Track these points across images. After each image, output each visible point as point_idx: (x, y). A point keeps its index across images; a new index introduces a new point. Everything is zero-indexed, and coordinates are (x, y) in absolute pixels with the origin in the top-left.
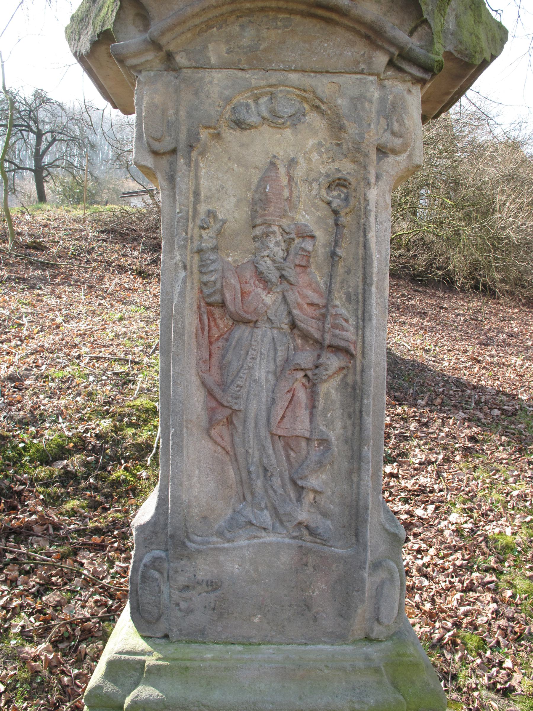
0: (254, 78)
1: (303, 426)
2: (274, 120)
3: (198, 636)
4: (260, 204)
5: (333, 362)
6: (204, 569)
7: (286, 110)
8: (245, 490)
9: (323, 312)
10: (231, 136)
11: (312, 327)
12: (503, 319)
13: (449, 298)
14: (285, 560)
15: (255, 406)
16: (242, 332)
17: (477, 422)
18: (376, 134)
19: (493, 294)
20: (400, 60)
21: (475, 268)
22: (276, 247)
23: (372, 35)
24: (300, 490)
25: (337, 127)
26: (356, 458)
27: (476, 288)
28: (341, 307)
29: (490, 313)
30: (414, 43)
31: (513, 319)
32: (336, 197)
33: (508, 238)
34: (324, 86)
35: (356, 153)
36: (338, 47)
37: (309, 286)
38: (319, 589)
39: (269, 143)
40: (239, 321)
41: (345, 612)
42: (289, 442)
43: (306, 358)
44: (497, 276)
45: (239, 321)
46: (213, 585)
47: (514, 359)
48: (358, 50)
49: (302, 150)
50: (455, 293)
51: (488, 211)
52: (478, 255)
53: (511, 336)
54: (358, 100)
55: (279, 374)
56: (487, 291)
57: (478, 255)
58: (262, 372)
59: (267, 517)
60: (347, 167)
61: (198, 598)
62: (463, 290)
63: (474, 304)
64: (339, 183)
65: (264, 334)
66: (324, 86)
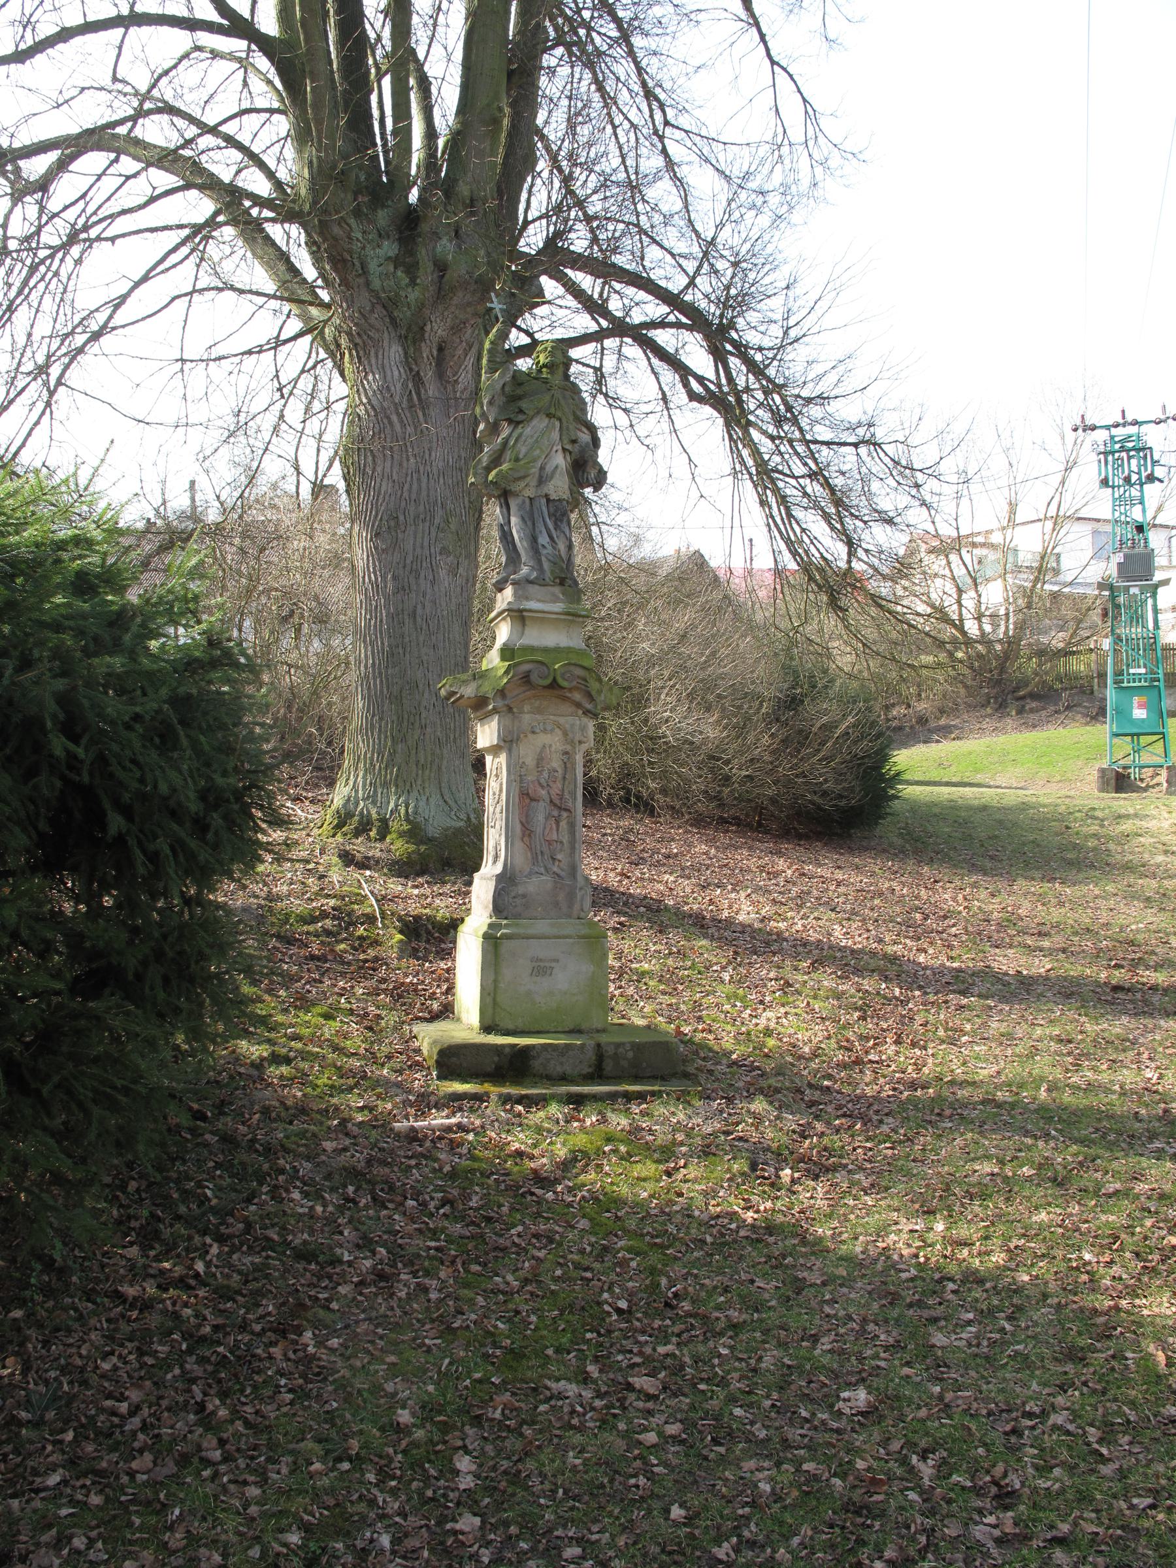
0: (538, 717)
1: (555, 837)
2: (545, 731)
3: (517, 916)
4: (540, 761)
5: (565, 814)
6: (521, 890)
7: (549, 728)
8: (535, 860)
9: (561, 797)
10: (530, 736)
11: (558, 802)
12: (661, 840)
13: (593, 815)
14: (549, 886)
15: (539, 830)
16: (534, 804)
17: (625, 914)
18: (578, 737)
19: (652, 813)
20: (586, 712)
21: (626, 775)
22: (545, 774)
23: (578, 705)
24: (554, 859)
25: (565, 734)
26: (573, 848)
27: (628, 801)
28: (567, 796)
29: (646, 833)
30: (589, 706)
31: (673, 840)
32: (565, 758)
33: (665, 736)
34: (562, 720)
35: (572, 743)
36: (567, 708)
37: (556, 788)
38: (561, 897)
39: (543, 739)
40: (532, 800)
41: (570, 906)
42: (549, 843)
43: (556, 813)
44: (653, 785)
45: (532, 800)
46: (524, 896)
47: (667, 876)
48: (573, 708)
49: (554, 741)
50: (599, 807)
51: (640, 702)
52: (628, 757)
53: (668, 857)
54: (572, 725)
55: (547, 819)
56: (644, 806)
57: (628, 757)
58: (541, 817)
59: (542, 870)
60: (569, 748)
61: (518, 901)
62: (610, 805)
63: (626, 823)
64: (566, 753)
65: (541, 803)
66: (562, 720)
